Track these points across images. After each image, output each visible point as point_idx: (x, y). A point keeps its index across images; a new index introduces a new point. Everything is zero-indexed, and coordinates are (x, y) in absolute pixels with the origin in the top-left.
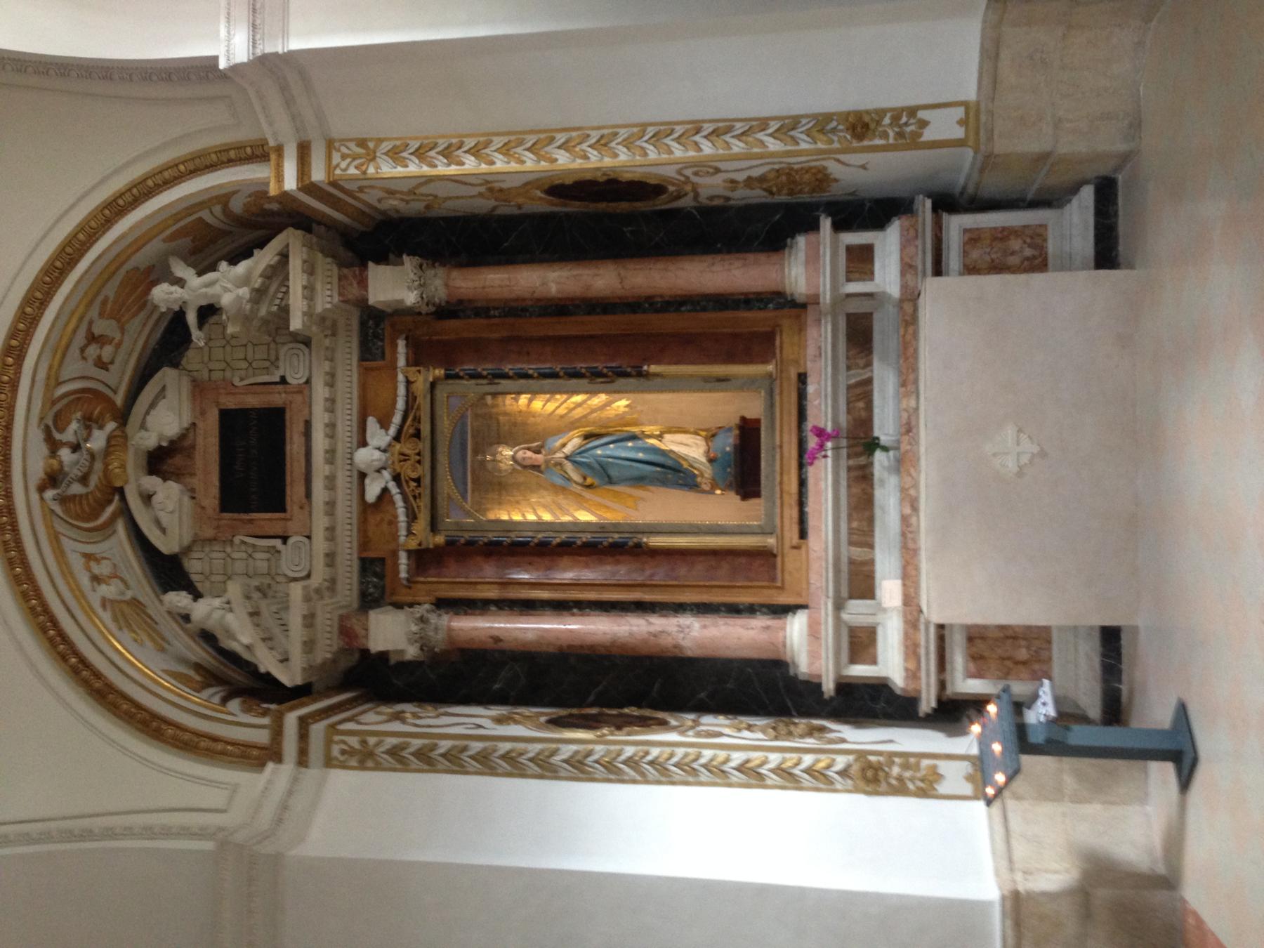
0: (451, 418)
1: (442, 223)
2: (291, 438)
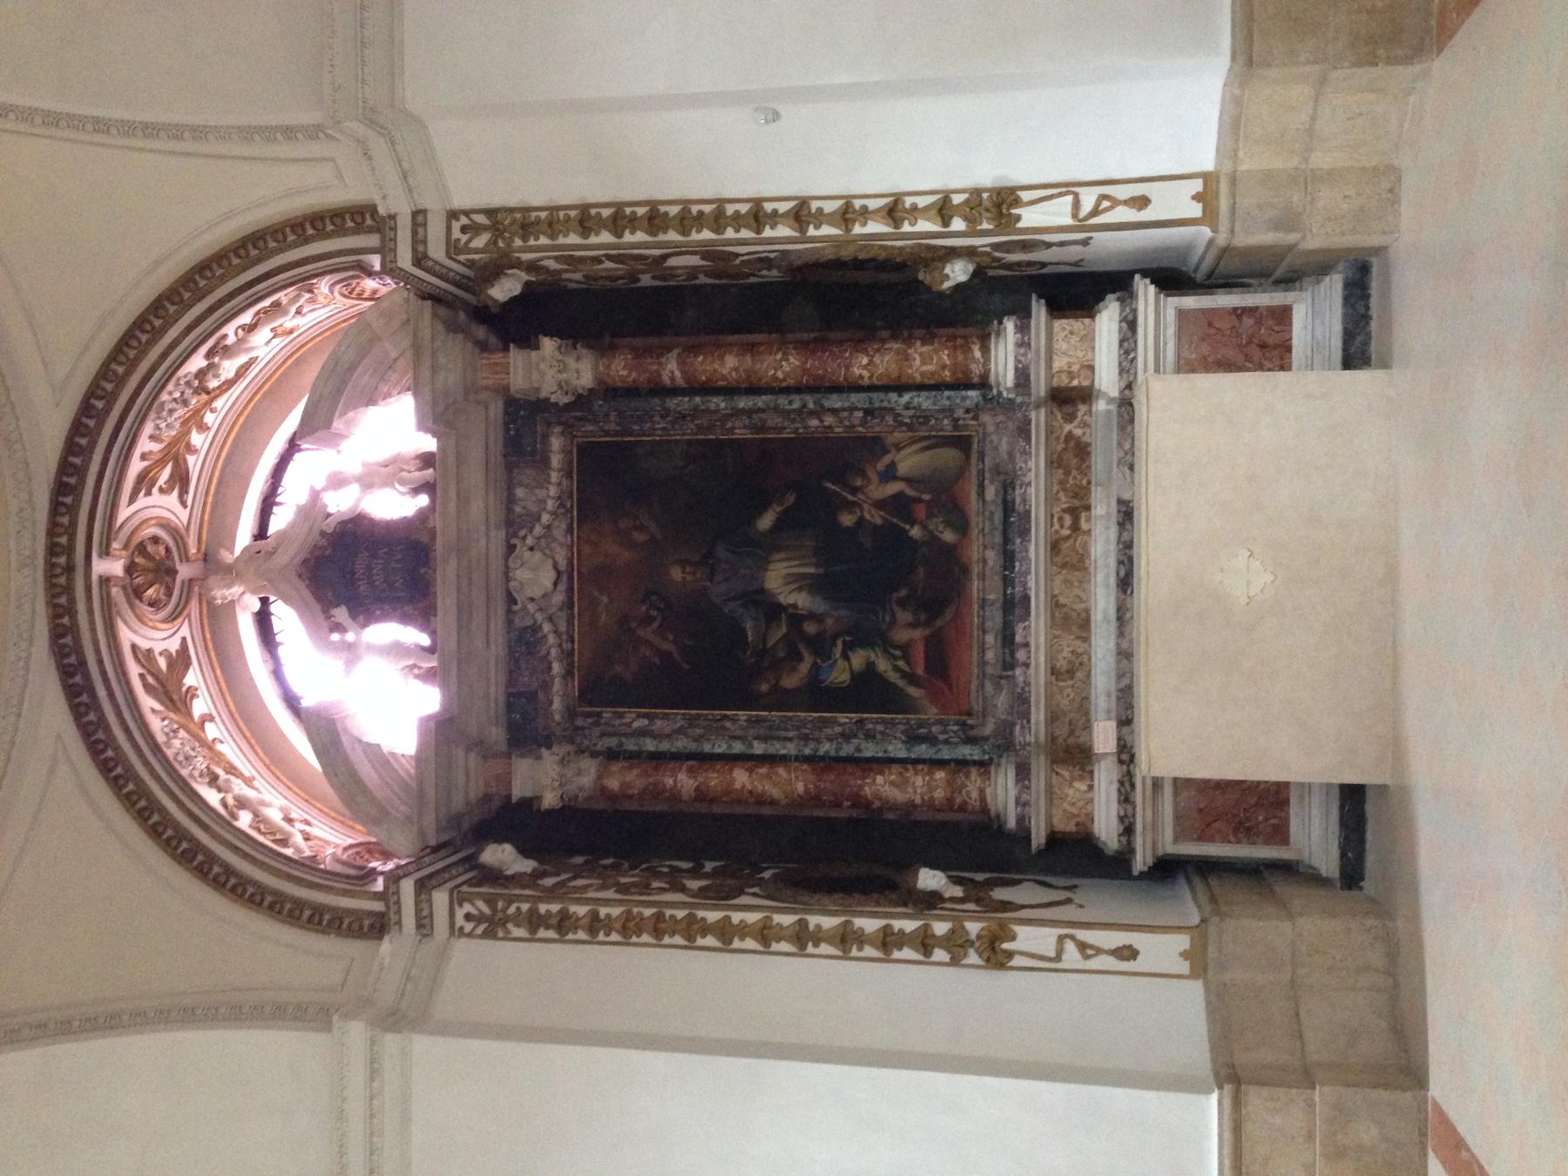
0: (1132, 355)
1: (976, 281)
2: (1100, 349)
